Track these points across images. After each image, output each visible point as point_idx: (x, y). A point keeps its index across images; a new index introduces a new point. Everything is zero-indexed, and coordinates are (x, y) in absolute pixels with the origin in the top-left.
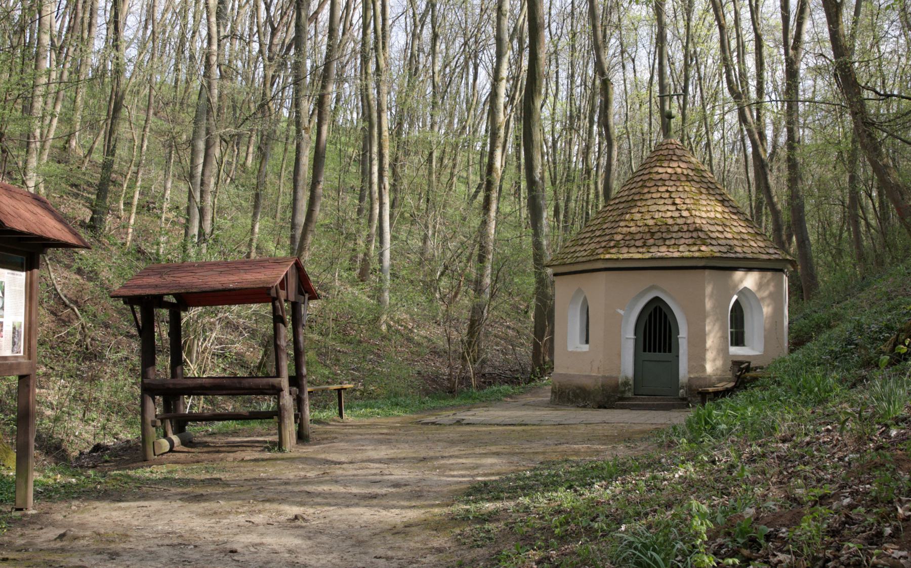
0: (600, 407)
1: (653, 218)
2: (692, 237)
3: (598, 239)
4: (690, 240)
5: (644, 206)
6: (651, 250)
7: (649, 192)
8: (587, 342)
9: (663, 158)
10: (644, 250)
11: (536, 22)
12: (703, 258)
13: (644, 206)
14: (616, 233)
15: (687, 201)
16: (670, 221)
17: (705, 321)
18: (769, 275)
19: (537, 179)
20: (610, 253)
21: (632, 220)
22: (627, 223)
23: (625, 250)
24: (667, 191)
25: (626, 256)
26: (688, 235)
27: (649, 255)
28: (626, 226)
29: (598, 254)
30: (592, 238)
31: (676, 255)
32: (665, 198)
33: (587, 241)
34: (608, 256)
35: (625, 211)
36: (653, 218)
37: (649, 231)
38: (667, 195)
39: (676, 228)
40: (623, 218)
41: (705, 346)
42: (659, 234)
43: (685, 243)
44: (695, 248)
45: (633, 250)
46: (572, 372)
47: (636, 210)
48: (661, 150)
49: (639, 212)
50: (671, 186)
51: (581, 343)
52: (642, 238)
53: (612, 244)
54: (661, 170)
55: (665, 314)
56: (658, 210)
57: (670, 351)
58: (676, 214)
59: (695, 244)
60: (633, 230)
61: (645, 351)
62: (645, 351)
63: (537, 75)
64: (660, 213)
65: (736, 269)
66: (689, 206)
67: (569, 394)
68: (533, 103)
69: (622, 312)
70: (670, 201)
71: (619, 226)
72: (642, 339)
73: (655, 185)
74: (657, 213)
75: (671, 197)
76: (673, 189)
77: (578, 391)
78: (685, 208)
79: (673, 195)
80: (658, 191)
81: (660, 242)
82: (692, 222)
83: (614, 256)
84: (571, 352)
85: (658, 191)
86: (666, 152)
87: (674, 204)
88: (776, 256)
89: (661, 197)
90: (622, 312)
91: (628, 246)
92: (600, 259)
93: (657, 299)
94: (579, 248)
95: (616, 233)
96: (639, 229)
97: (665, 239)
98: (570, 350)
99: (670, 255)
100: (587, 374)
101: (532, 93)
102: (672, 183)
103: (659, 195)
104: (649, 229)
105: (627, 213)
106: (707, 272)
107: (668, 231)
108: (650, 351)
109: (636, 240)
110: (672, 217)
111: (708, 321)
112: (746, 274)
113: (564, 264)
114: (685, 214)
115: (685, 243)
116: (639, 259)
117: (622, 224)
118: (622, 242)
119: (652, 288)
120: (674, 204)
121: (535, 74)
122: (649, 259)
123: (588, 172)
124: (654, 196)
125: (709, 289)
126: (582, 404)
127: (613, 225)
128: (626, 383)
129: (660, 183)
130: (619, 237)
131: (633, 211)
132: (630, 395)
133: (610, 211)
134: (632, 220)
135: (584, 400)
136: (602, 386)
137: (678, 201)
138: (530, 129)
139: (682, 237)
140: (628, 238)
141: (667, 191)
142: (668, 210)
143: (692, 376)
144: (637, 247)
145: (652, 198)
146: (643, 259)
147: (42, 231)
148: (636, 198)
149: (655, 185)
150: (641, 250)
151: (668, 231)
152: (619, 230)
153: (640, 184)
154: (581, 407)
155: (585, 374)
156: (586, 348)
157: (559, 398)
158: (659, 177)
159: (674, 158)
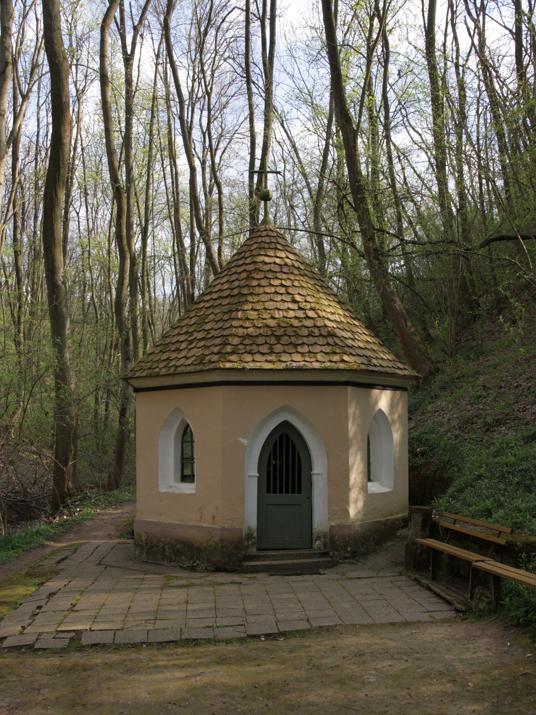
0: (218, 569)
1: (273, 318)
2: (328, 344)
3: (202, 343)
4: (326, 347)
5: (258, 301)
6: (283, 359)
7: (259, 286)
8: (301, 505)
9: (266, 246)
10: (272, 358)
11: (61, 101)
12: (351, 370)
13: (258, 301)
14: (230, 335)
15: (309, 299)
16: (296, 323)
17: (347, 453)
18: (398, 393)
19: (60, 283)
20: (229, 361)
21: (247, 319)
22: (241, 323)
23: (248, 358)
24: (282, 285)
25: (252, 365)
26: (321, 341)
27: (282, 366)
28: (241, 327)
29: (210, 362)
30: (191, 342)
31: (316, 365)
32: (282, 294)
33: (183, 346)
34: (228, 365)
35: (234, 307)
36: (273, 318)
37: (273, 334)
38: (283, 290)
39: (305, 332)
40: (233, 316)
41: (348, 484)
42: (286, 338)
43: (322, 351)
44: (336, 358)
45: (258, 357)
46: (167, 520)
47: (249, 306)
48: (260, 236)
49: (253, 309)
50: (285, 280)
51: (176, 481)
52: (266, 343)
53: (229, 349)
54: (267, 260)
55: (293, 443)
56: (277, 308)
57: (299, 492)
58: (301, 314)
59: (334, 353)
60: (251, 330)
61: (268, 492)
62: (268, 492)
63: (61, 162)
64: (281, 312)
65: (372, 386)
66: (313, 305)
67: (164, 548)
68: (56, 195)
69: (244, 441)
70: (288, 298)
71: (231, 326)
72: (265, 476)
73: (265, 277)
74: (276, 312)
75: (288, 293)
76: (288, 283)
77: (179, 546)
78: (309, 307)
79: (290, 290)
80: (271, 285)
81: (291, 349)
82: (322, 324)
83: (236, 365)
84: (165, 494)
85: (271, 285)
86: (267, 240)
87: (294, 301)
88: (406, 372)
89: (276, 293)
90: (244, 441)
91: (250, 353)
92: (220, 369)
93: (285, 424)
94: (173, 355)
95: (230, 335)
96: (258, 331)
97: (296, 345)
98: (163, 490)
99: (309, 366)
100: (194, 523)
101: (55, 183)
102: (285, 276)
103: (273, 290)
104: (273, 331)
105: (238, 310)
106: (350, 389)
107: (297, 335)
108: (275, 492)
109: (258, 345)
110: (296, 318)
111: (352, 451)
112: (381, 392)
113: (158, 375)
114: (311, 314)
115: (322, 351)
116: (272, 370)
117: (235, 323)
118: (241, 347)
119: (284, 409)
120: (294, 301)
121: (59, 161)
122: (284, 370)
123: (92, 286)
124: (268, 290)
125: (352, 410)
126: (187, 564)
127: (220, 324)
128: (249, 536)
129: (270, 275)
130: (236, 341)
131: (245, 307)
132: (253, 551)
133: (208, 308)
134: (247, 319)
135: (191, 558)
136: (221, 541)
137: (298, 298)
138: (52, 225)
139: (316, 343)
140: (246, 342)
141: (282, 285)
142: (289, 308)
143: (333, 524)
144: (263, 354)
145: (265, 293)
146: (276, 370)
147: (353, 466)
148: (245, 291)
149: (265, 277)
150: (269, 358)
151: (297, 335)
152: (234, 331)
153: (244, 275)
154: (185, 569)
155: (190, 524)
156: (188, 488)
157: (148, 552)
158: (267, 267)
159: (279, 247)
